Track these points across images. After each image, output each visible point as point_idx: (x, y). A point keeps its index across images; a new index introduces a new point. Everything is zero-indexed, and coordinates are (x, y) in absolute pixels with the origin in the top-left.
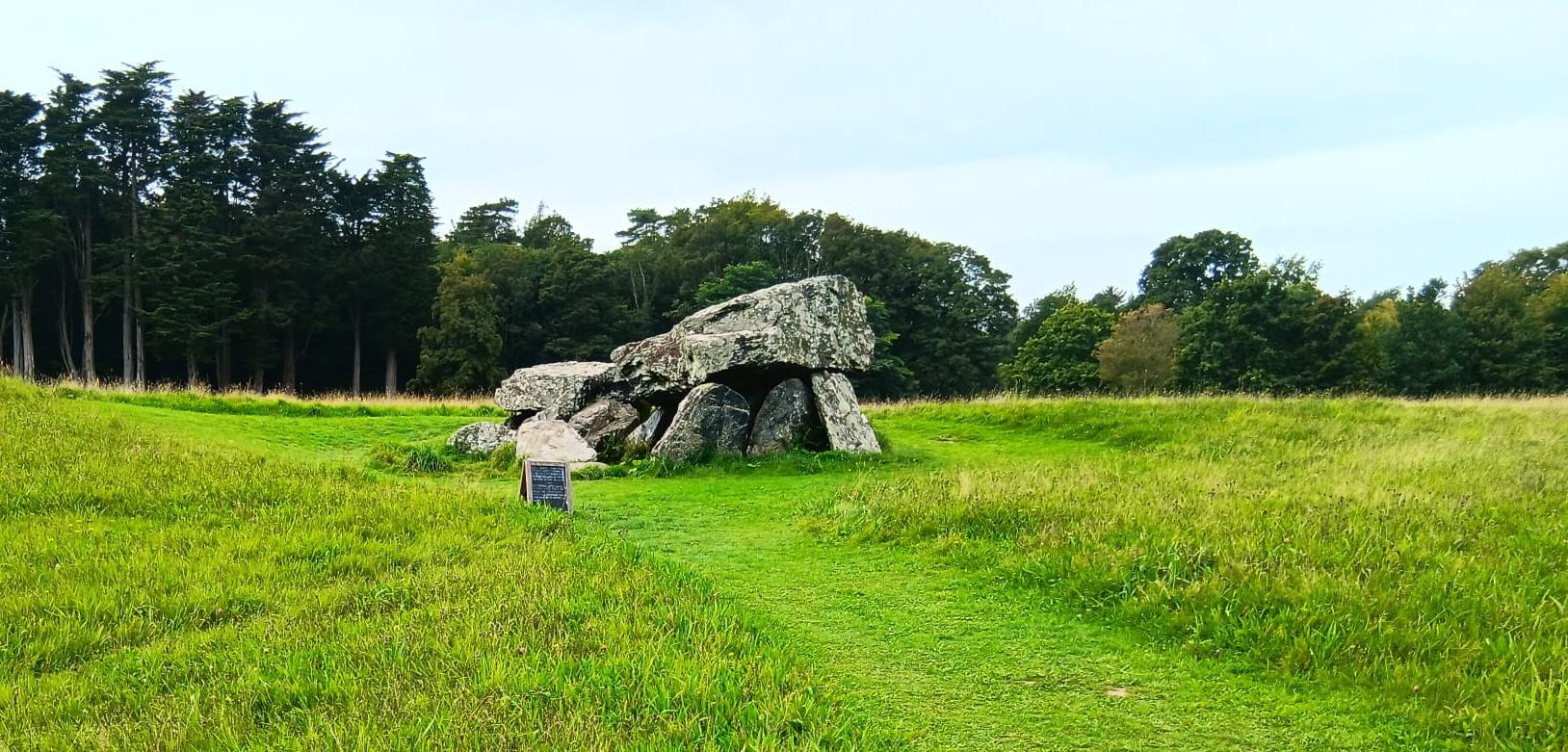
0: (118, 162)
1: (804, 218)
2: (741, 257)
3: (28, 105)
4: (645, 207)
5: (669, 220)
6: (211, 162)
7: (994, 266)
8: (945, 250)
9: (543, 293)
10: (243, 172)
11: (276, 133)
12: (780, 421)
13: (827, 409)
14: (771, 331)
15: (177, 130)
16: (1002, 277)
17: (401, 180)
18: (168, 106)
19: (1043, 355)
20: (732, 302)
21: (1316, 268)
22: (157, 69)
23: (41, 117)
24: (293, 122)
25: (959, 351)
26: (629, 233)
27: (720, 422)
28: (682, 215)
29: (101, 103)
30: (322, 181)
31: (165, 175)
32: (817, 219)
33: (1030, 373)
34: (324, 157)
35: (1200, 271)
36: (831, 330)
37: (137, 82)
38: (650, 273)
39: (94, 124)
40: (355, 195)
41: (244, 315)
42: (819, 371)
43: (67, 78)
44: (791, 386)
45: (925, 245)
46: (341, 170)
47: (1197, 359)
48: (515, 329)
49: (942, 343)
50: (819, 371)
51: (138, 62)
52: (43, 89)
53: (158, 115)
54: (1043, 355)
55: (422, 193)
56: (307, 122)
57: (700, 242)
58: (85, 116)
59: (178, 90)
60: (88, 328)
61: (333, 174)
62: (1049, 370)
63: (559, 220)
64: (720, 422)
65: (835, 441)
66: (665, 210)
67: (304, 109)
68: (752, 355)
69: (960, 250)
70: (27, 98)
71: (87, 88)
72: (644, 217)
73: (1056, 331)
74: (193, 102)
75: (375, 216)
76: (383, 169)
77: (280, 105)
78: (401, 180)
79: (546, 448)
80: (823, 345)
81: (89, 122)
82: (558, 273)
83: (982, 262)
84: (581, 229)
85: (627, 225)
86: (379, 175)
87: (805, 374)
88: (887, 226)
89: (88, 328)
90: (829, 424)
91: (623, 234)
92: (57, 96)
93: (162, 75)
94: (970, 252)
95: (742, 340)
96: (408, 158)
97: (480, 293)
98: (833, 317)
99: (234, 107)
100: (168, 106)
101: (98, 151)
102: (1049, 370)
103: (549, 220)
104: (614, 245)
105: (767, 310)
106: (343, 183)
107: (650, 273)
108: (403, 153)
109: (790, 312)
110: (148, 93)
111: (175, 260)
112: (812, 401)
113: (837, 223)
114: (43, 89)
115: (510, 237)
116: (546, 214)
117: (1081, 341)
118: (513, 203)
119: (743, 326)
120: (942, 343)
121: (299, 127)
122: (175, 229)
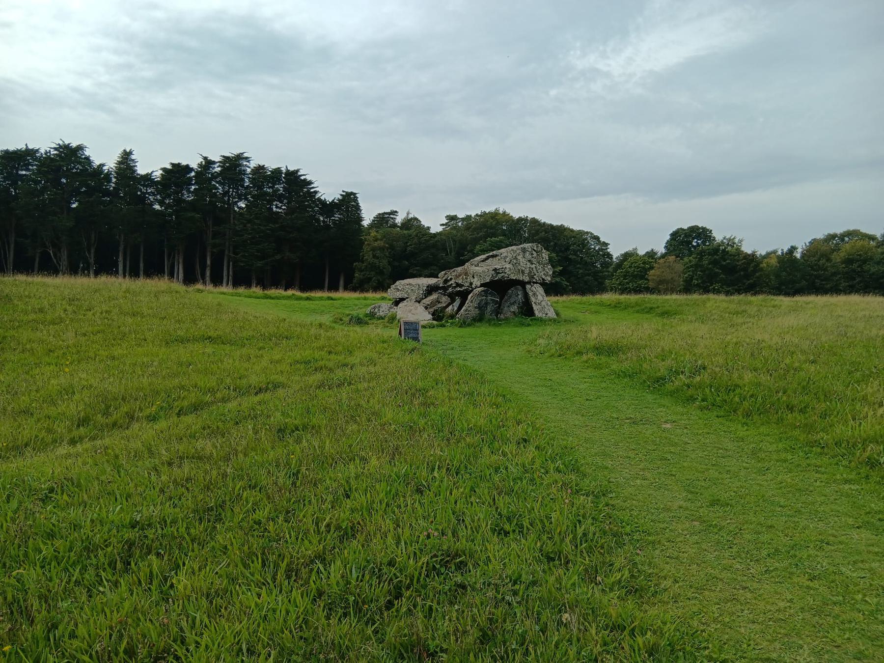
0: (226, 193)
1: (520, 219)
2: (494, 235)
3: (188, 169)
4: (452, 214)
5: (463, 219)
6: (266, 194)
7: (602, 240)
8: (581, 233)
9: (409, 249)
10: (280, 198)
11: (295, 183)
12: (513, 304)
13: (533, 299)
14: (508, 266)
15: (252, 181)
16: (606, 244)
17: (349, 202)
18: (249, 170)
19: (625, 277)
20: (491, 254)
21: (740, 241)
22: (245, 155)
23: (193, 174)
24: (302, 178)
25: (589, 275)
26: (446, 224)
27: (486, 304)
28: (468, 217)
29: (219, 169)
30: (314, 202)
31: (246, 199)
32: (526, 219)
33: (620, 284)
34: (316, 192)
35: (691, 243)
36: (533, 266)
37: (236, 160)
38: (454, 241)
39: (216, 177)
40: (328, 208)
41: (278, 257)
42: (529, 283)
43: (205, 158)
44: (517, 289)
45: (572, 231)
46: (322, 198)
47: (692, 279)
48: (396, 264)
49: (581, 271)
50: (529, 283)
51: (236, 152)
52: (194, 163)
53: (244, 174)
54: (625, 277)
55: (358, 207)
56: (308, 178)
57: (475, 229)
58: (212, 174)
59: (253, 164)
60: (209, 262)
61: (319, 199)
62: (628, 283)
63: (416, 219)
64: (486, 304)
65: (536, 312)
66: (461, 215)
67: (307, 173)
68: (500, 276)
69: (587, 233)
70: (187, 166)
71: (214, 163)
72: (452, 218)
73: (630, 267)
74: (260, 169)
75: (337, 216)
76: (340, 197)
77: (298, 171)
78: (349, 202)
79: (410, 315)
80: (530, 272)
81: (215, 176)
82: (416, 240)
83: (597, 238)
84: (425, 223)
85: (445, 221)
86: (339, 200)
87: (523, 284)
88: (555, 223)
89: (209, 262)
90: (534, 305)
91: (442, 225)
92: (200, 165)
93: (247, 158)
94: (592, 234)
95: (495, 270)
96: (352, 193)
97: (382, 249)
98: (534, 261)
99: (278, 171)
100: (249, 170)
101: (217, 188)
102: (628, 283)
103: (412, 219)
104: (440, 229)
105: (506, 257)
106: (323, 203)
107: (454, 241)
108: (350, 191)
109: (516, 258)
110: (240, 165)
111: (249, 234)
112: (526, 295)
113: (534, 221)
114: (194, 163)
115: (394, 225)
116: (411, 216)
117: (640, 271)
118: (396, 212)
119: (495, 264)
120: (581, 271)
121: (305, 180)
122: (249, 221)
